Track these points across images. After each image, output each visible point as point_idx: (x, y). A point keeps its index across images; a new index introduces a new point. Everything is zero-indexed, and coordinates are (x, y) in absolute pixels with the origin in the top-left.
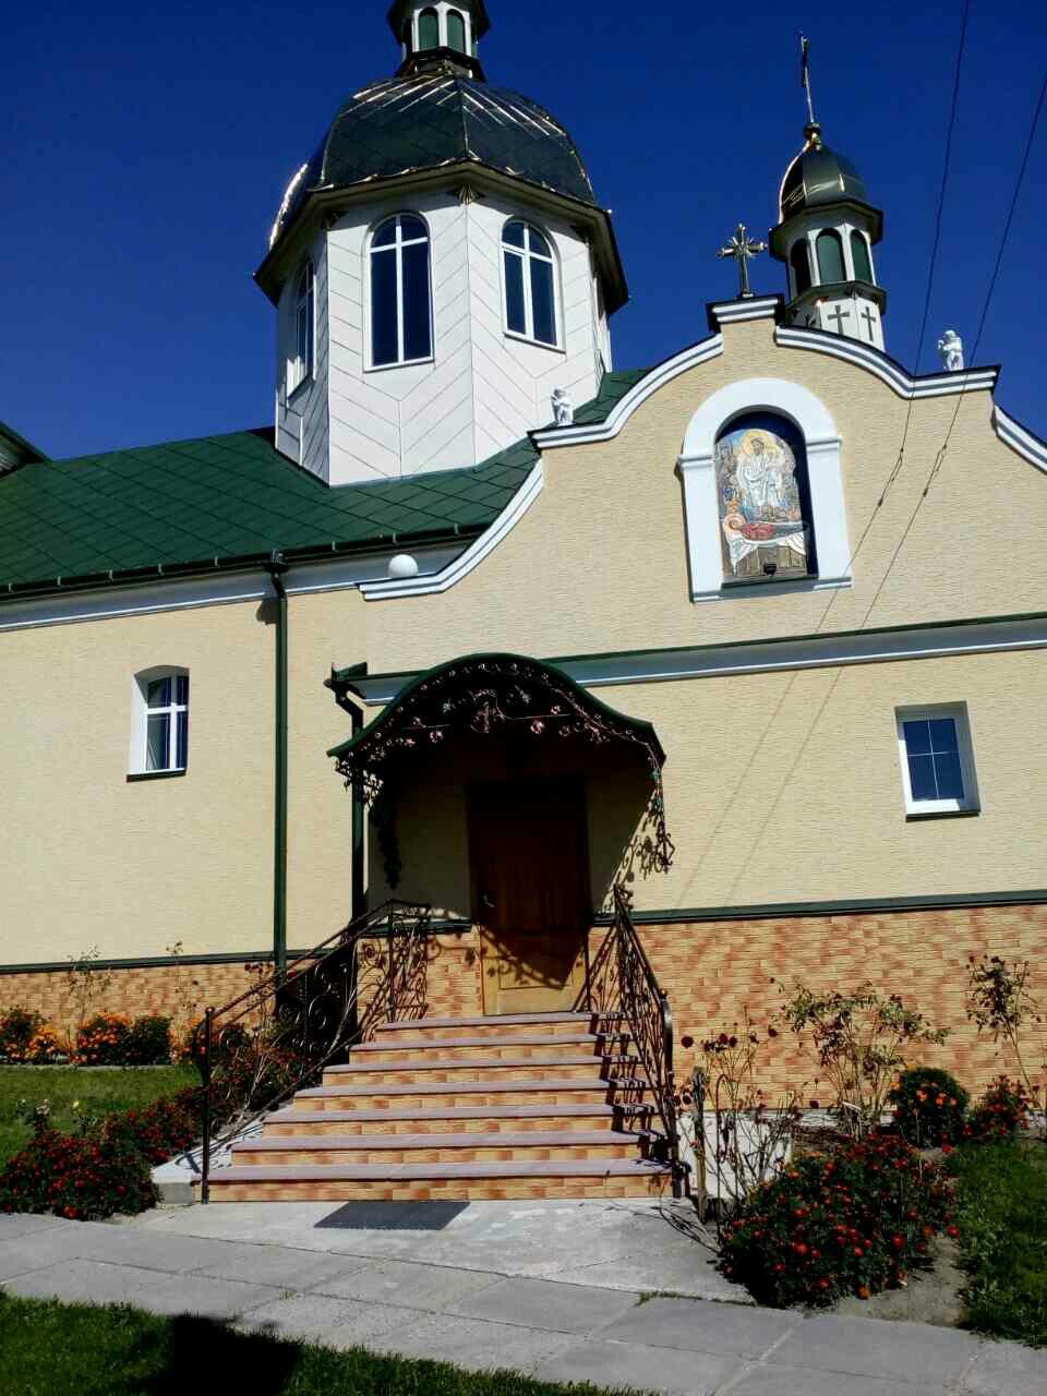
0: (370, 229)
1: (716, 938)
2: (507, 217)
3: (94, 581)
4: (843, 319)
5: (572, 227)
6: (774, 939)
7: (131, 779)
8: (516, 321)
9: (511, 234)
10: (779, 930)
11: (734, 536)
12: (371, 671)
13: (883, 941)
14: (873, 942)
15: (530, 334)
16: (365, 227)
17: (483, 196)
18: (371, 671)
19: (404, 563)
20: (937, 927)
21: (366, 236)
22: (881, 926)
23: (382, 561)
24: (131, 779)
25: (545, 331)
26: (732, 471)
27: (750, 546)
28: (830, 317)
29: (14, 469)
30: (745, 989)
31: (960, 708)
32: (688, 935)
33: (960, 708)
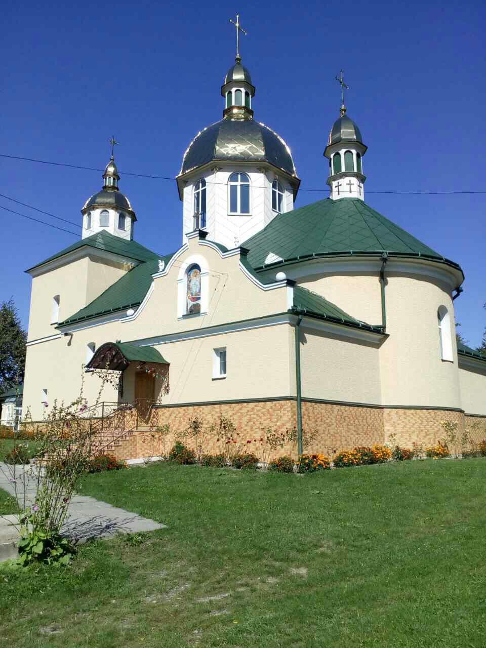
0: (194, 185)
1: (173, 412)
2: (231, 173)
3: (108, 312)
4: (352, 186)
5: (258, 169)
6: (184, 412)
7: (213, 380)
8: (233, 208)
9: (233, 178)
10: (184, 410)
11: (189, 301)
12: (121, 342)
13: (203, 413)
14: (201, 413)
15: (239, 212)
16: (192, 185)
17: (221, 169)
18: (121, 342)
19: (130, 312)
20: (213, 409)
21: (192, 189)
22: (203, 409)
23: (124, 313)
24: (213, 380)
25: (245, 209)
26: (190, 282)
27: (192, 303)
28: (350, 181)
29: (137, 266)
30: (178, 425)
31: (225, 348)
32: (169, 411)
33: (225, 348)
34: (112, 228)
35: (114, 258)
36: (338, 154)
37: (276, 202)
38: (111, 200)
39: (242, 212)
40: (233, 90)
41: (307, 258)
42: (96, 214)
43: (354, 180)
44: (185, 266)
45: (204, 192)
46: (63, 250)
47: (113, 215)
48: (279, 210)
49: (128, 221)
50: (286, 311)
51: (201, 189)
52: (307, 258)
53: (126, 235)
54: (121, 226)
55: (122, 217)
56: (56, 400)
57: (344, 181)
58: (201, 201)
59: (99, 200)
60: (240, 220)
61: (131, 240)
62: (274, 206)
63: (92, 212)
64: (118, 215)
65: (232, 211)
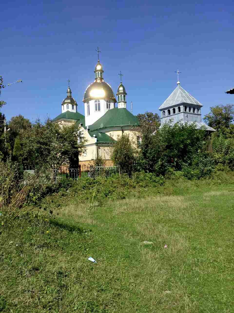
8: (96, 110)
25: (99, 110)
34: (70, 110)
35: (71, 120)
36: (119, 96)
37: (108, 106)
38: (69, 101)
39: (99, 110)
40: (97, 72)
41: (106, 128)
42: (65, 105)
43: (123, 103)
44: (116, 95)
45: (89, 105)
46: (56, 116)
47: (70, 105)
48: (109, 108)
49: (75, 107)
50: (95, 143)
51: (88, 105)
52: (106, 128)
53: (74, 111)
54: (73, 108)
55: (73, 106)
56: (228, 93)
57: (120, 104)
58: (89, 107)
59: (66, 101)
60: (98, 112)
61: (76, 112)
62: (107, 107)
63: (64, 105)
64: (72, 105)
65: (96, 110)
